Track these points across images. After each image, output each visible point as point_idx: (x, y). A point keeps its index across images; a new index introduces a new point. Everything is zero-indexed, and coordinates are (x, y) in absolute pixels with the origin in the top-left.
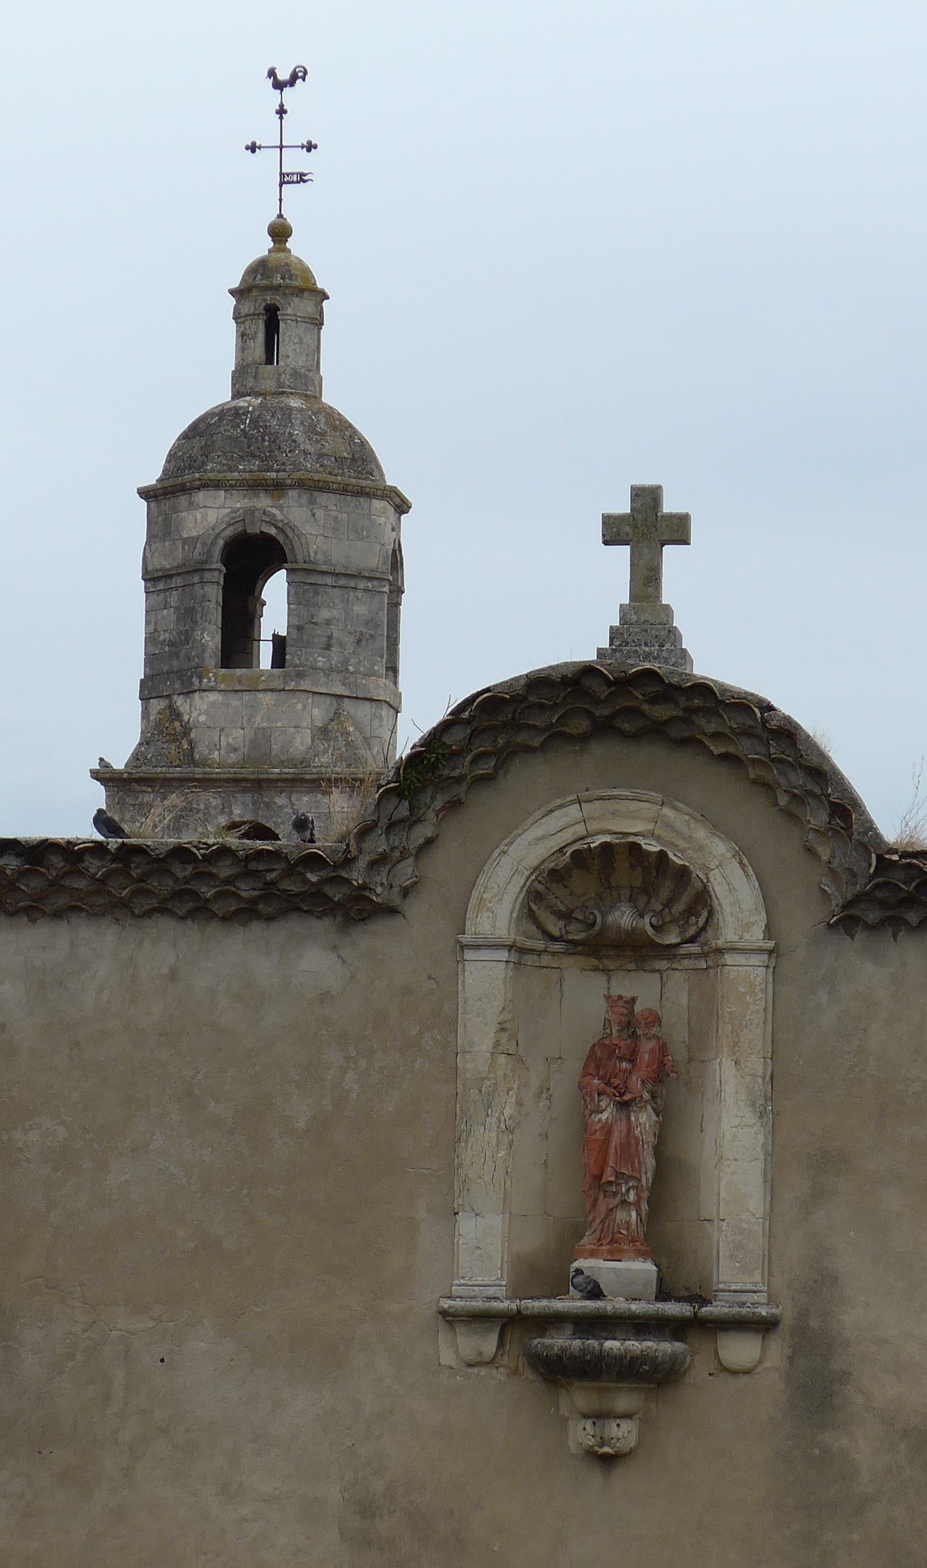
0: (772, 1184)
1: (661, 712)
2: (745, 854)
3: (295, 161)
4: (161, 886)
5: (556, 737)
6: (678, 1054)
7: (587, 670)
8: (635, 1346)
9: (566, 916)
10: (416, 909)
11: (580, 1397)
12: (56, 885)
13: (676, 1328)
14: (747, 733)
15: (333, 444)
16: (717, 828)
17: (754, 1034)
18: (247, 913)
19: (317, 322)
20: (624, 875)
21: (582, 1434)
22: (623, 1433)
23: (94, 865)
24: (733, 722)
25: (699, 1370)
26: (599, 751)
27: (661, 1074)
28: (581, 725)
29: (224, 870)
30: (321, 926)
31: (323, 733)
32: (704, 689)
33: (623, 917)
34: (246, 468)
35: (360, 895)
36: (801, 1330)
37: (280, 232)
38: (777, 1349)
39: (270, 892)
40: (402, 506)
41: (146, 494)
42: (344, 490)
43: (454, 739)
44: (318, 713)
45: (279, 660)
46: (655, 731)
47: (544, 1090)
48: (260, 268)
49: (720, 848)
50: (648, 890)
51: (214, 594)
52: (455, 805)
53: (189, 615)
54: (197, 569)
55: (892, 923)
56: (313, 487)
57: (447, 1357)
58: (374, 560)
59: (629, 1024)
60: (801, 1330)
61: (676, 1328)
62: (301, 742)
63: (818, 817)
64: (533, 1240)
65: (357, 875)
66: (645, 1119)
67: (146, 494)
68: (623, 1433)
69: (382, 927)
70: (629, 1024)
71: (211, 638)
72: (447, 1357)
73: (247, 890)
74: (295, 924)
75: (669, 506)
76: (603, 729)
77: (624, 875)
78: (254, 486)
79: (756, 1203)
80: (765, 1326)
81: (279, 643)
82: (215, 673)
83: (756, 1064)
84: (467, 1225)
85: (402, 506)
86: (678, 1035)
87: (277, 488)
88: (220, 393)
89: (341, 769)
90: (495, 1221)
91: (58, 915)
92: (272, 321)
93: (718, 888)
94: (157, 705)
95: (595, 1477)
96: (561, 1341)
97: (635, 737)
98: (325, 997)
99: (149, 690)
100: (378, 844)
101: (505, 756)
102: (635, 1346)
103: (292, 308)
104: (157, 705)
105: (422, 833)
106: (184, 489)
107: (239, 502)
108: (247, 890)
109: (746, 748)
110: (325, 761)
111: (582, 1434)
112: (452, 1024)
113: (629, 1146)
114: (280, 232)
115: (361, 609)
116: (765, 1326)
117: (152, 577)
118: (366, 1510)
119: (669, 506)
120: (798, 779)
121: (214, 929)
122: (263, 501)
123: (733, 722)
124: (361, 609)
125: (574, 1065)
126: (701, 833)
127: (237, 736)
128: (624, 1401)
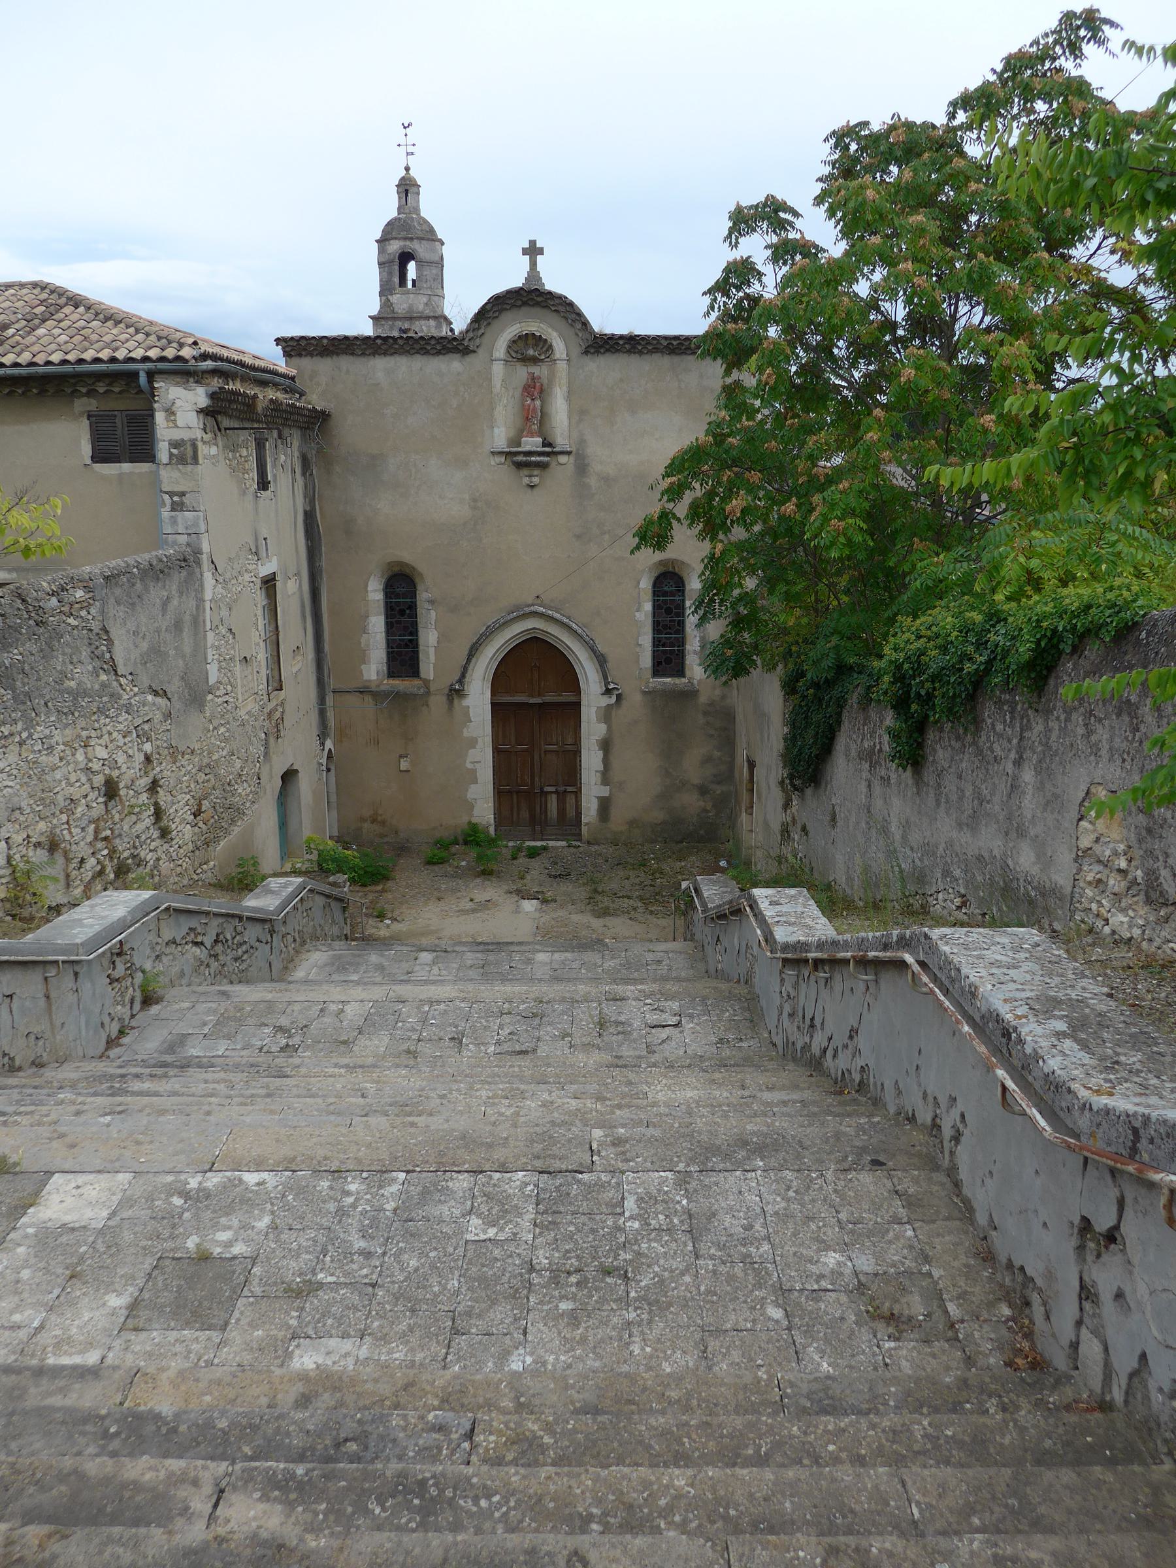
0: (569, 418)
1: (540, 299)
2: (561, 335)
3: (411, 149)
4: (417, 346)
5: (513, 306)
6: (545, 386)
7: (521, 289)
8: (539, 459)
9: (516, 352)
10: (480, 351)
11: (526, 471)
12: (391, 347)
13: (548, 454)
14: (561, 304)
15: (425, 227)
16: (554, 328)
17: (564, 381)
18: (439, 353)
19: (418, 194)
20: (530, 341)
21: (526, 480)
22: (536, 480)
23: (400, 342)
24: (557, 301)
25: (553, 464)
26: (525, 309)
27: (541, 391)
28: (519, 303)
29: (433, 342)
30: (458, 356)
31: (426, 304)
32: (550, 293)
33: (531, 352)
34: (403, 234)
35: (467, 348)
36: (577, 454)
37: (407, 169)
38: (572, 458)
39: (444, 347)
40: (443, 244)
41: (377, 241)
42: (428, 240)
43: (488, 307)
44: (425, 299)
45: (414, 285)
46: (538, 304)
47: (513, 396)
48: (403, 179)
49: (555, 334)
50: (537, 345)
51: (397, 268)
52: (489, 324)
53: (390, 273)
54: (391, 262)
55: (598, 352)
56: (420, 239)
57: (493, 463)
58: (437, 259)
59: (533, 379)
60: (577, 454)
61: (548, 454)
62: (421, 307)
63: (579, 326)
64: (512, 433)
65: (466, 343)
66: (538, 403)
67: (377, 241)
68: (536, 480)
69: (472, 356)
70: (533, 379)
71: (396, 280)
72: (493, 463)
73: (438, 347)
74: (451, 355)
75: (538, 245)
76: (525, 304)
77: (530, 341)
78: (405, 239)
79: (566, 423)
80: (569, 453)
81: (414, 281)
82: (399, 290)
83: (565, 388)
84: (496, 430)
85: (443, 244)
86: (545, 381)
87: (411, 239)
88: (395, 214)
89: (432, 314)
90: (503, 429)
91: (392, 354)
92: (407, 192)
93: (554, 344)
94: (384, 298)
95: (529, 490)
96: (520, 458)
97: (533, 306)
98: (459, 374)
99: (381, 294)
100: (471, 334)
101: (501, 311)
102: (539, 459)
103: (412, 190)
104: (384, 298)
105: (481, 331)
106: (387, 240)
107: (402, 243)
108: (438, 347)
109: (561, 308)
110: (427, 312)
111: (526, 480)
112: (490, 380)
113: (534, 409)
114: (407, 169)
115: (434, 271)
116: (569, 453)
117: (379, 264)
118: (475, 500)
119: (538, 245)
120: (573, 316)
121: (431, 357)
122: (408, 243)
123: (557, 301)
124: (434, 271)
125: (520, 390)
126: (550, 330)
127: (405, 306)
128: (536, 473)
